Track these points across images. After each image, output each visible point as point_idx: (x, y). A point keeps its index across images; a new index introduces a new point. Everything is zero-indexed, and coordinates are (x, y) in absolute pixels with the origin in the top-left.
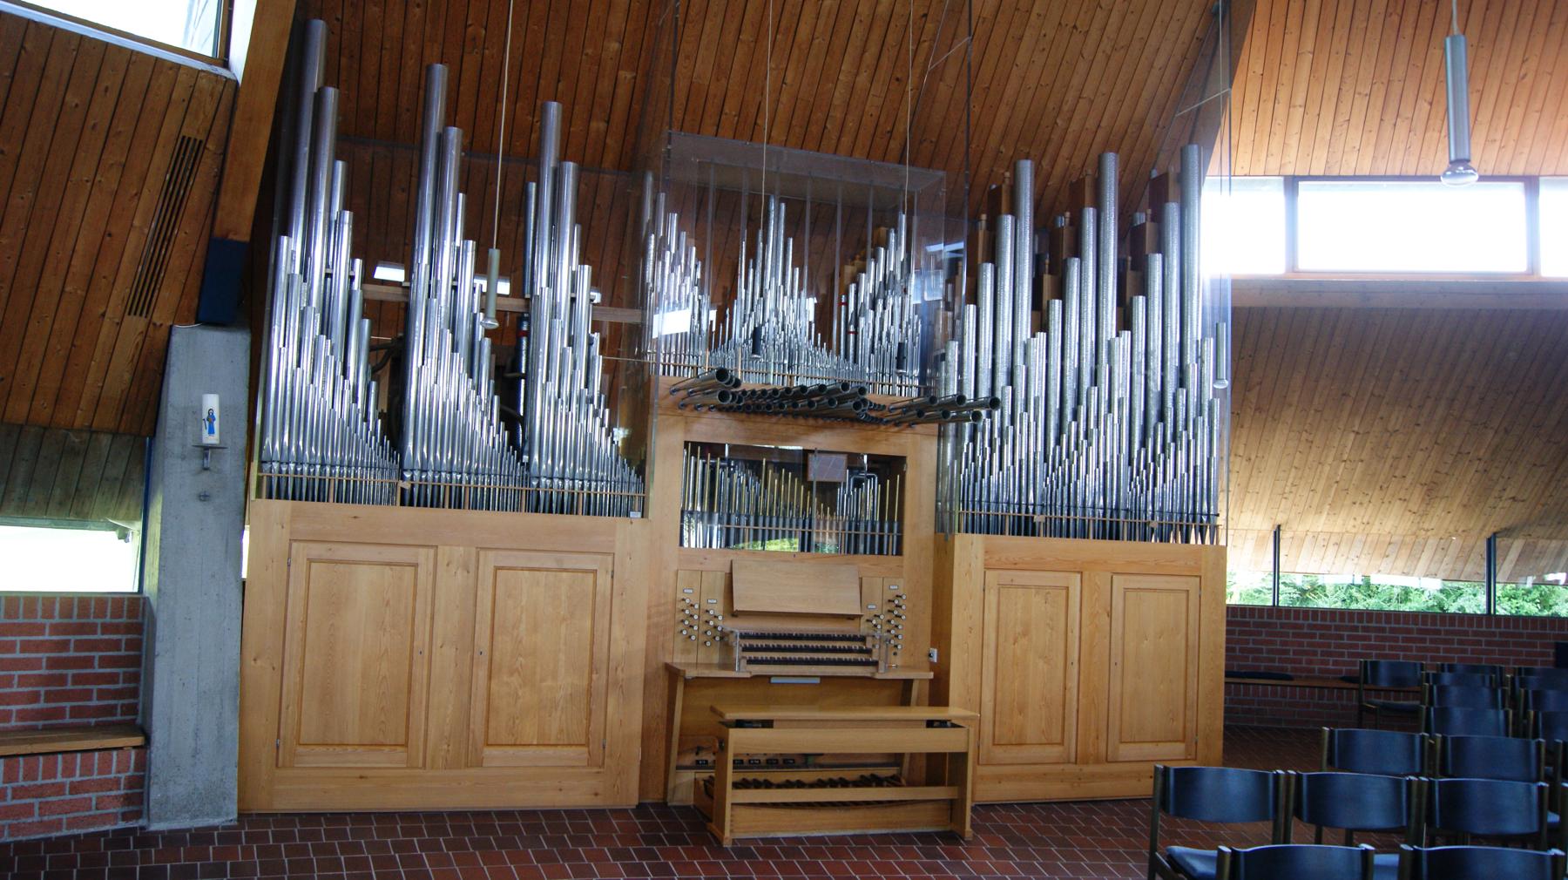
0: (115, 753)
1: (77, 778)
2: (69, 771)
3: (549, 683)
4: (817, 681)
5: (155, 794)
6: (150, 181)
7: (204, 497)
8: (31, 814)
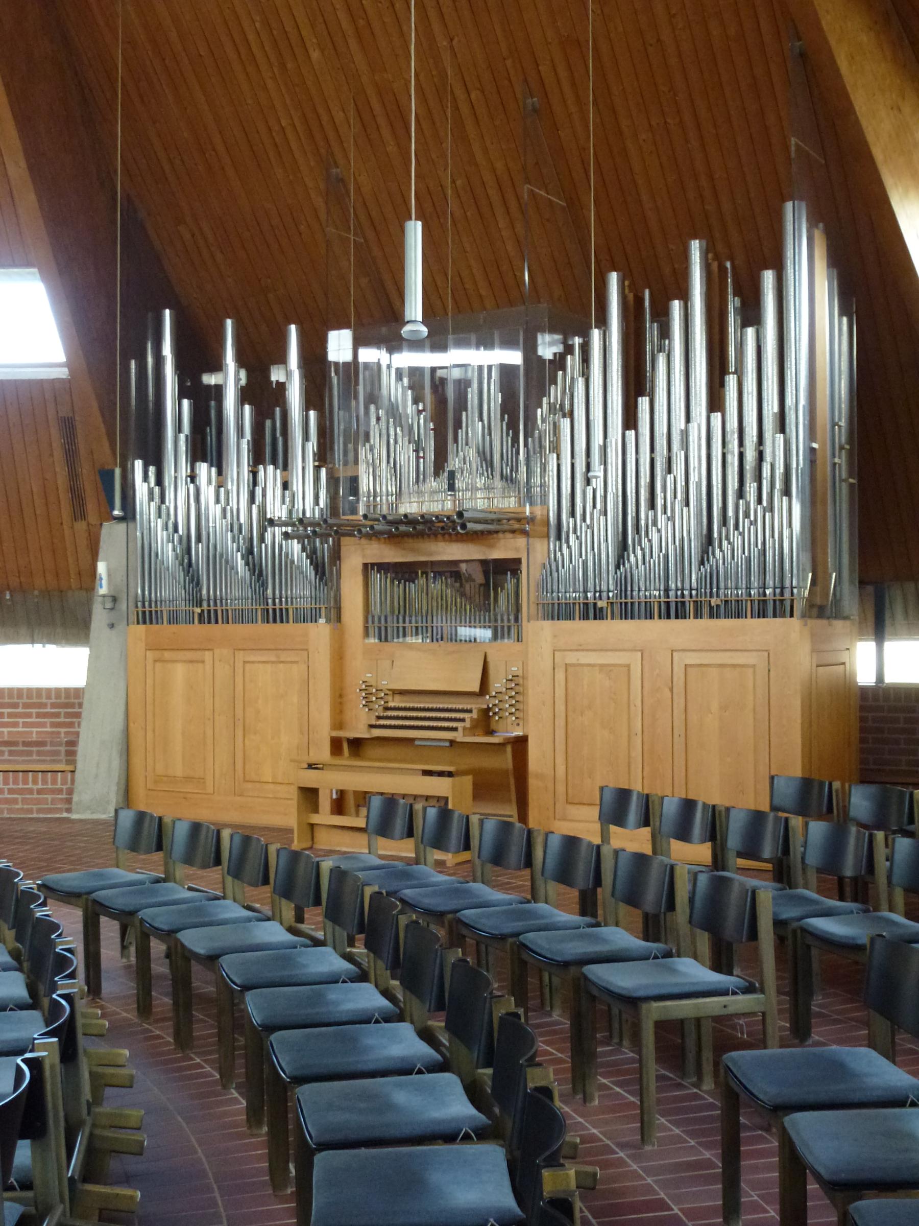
0: (30, 774)
1: (40, 786)
2: (35, 782)
4: (447, 744)
5: (75, 798)
6: (54, 445)
7: (112, 626)
8: (17, 803)
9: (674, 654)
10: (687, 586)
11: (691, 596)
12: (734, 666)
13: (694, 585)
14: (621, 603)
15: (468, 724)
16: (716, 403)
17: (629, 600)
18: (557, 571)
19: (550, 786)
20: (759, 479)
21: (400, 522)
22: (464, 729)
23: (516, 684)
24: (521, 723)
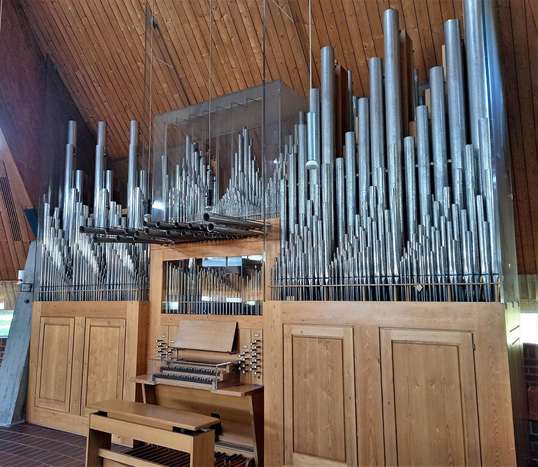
3: (105, 379)
9: (382, 330)
10: (389, 273)
11: (394, 282)
12: (438, 345)
13: (396, 272)
14: (335, 287)
15: (221, 378)
16: (406, 128)
17: (341, 285)
18: (286, 262)
19: (281, 434)
20: (450, 182)
21: (173, 228)
22: (219, 382)
23: (258, 345)
24: (261, 376)
